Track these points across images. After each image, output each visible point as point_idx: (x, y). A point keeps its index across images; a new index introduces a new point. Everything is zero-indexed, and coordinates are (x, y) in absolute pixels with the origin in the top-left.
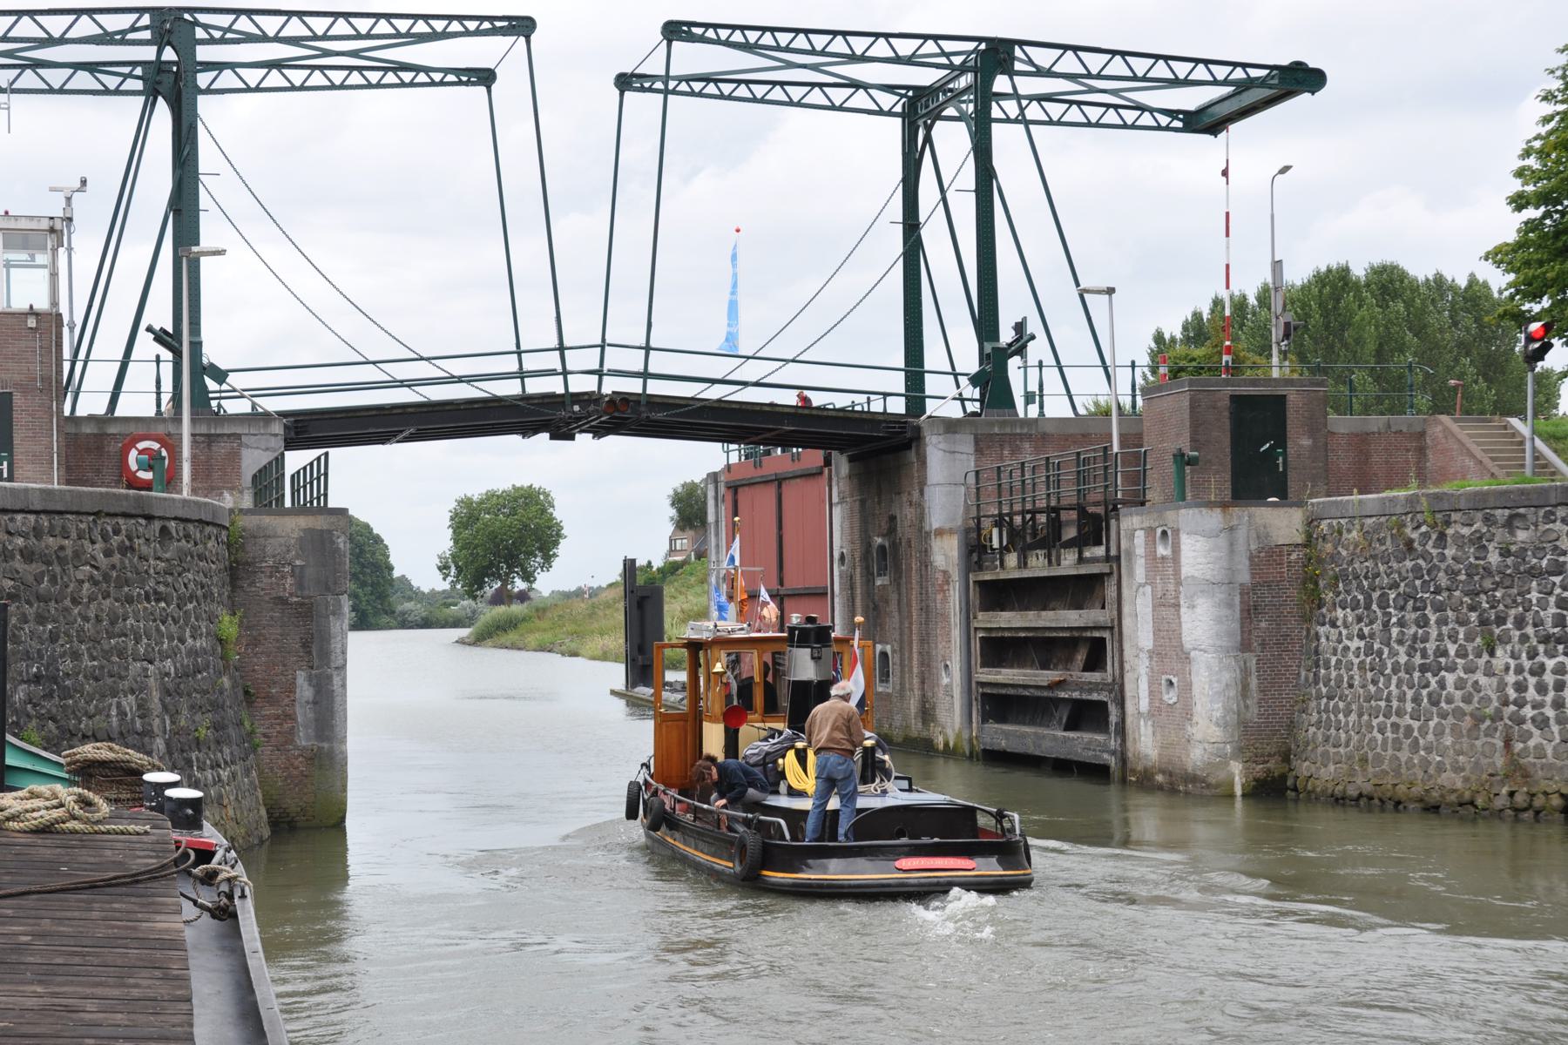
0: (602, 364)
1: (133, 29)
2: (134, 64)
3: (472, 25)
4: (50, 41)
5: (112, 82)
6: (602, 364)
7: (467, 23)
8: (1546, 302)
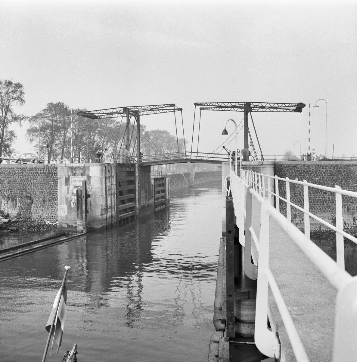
0: (196, 153)
1: (121, 110)
2: (293, 109)
3: (166, 106)
4: (216, 108)
5: (291, 111)
6: (196, 153)
7: (212, 105)
8: (91, 133)
